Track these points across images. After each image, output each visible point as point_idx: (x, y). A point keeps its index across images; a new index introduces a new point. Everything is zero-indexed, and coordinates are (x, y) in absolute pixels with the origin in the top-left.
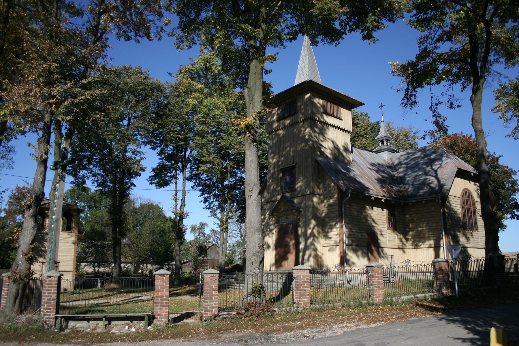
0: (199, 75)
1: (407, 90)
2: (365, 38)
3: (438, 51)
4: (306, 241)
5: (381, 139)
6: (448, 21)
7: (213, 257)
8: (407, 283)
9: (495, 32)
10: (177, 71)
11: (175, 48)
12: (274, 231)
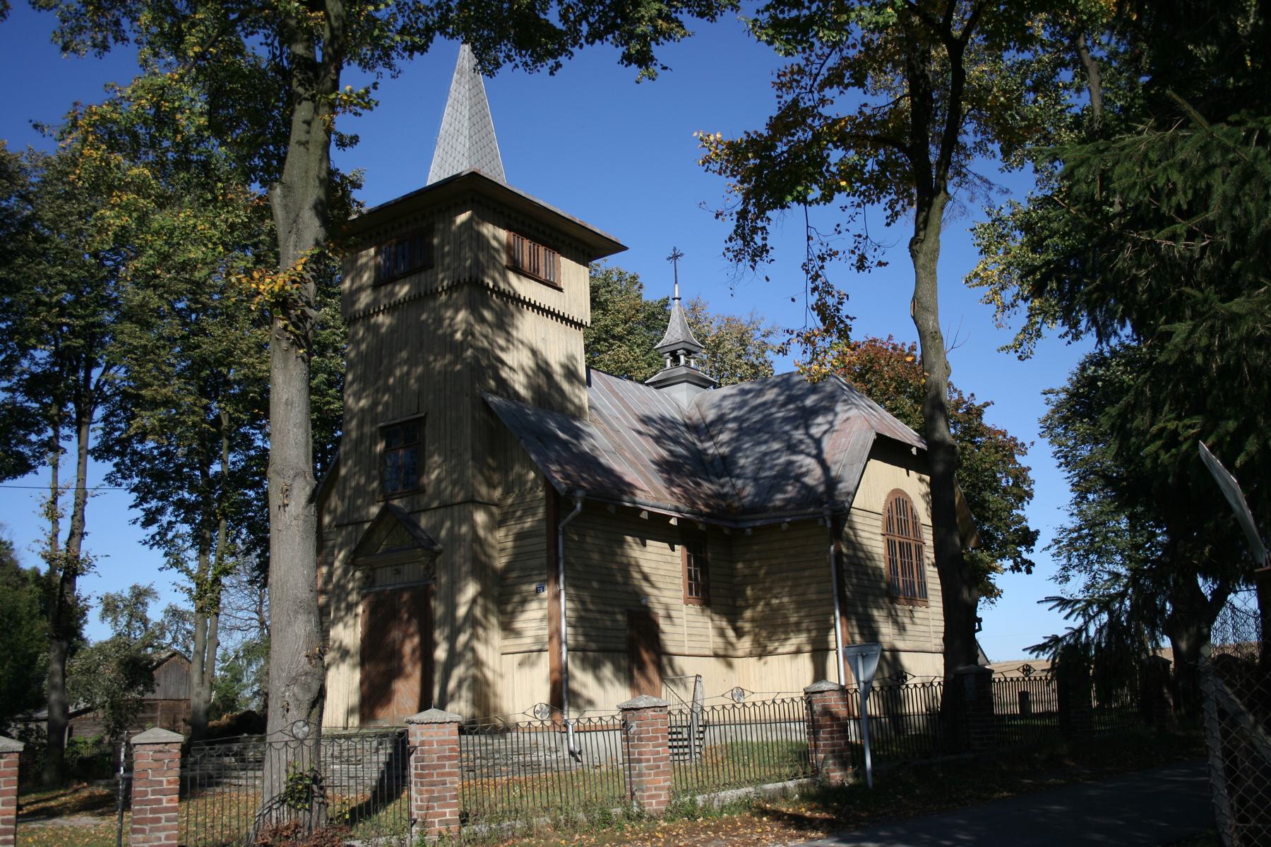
0: (135, 136)
1: (743, 215)
2: (628, 59)
3: (826, 111)
4: (452, 639)
5: (672, 348)
6: (857, 32)
7: (172, 693)
8: (733, 752)
9: (975, 72)
10: (64, 122)
11: (58, 49)
12: (360, 609)
